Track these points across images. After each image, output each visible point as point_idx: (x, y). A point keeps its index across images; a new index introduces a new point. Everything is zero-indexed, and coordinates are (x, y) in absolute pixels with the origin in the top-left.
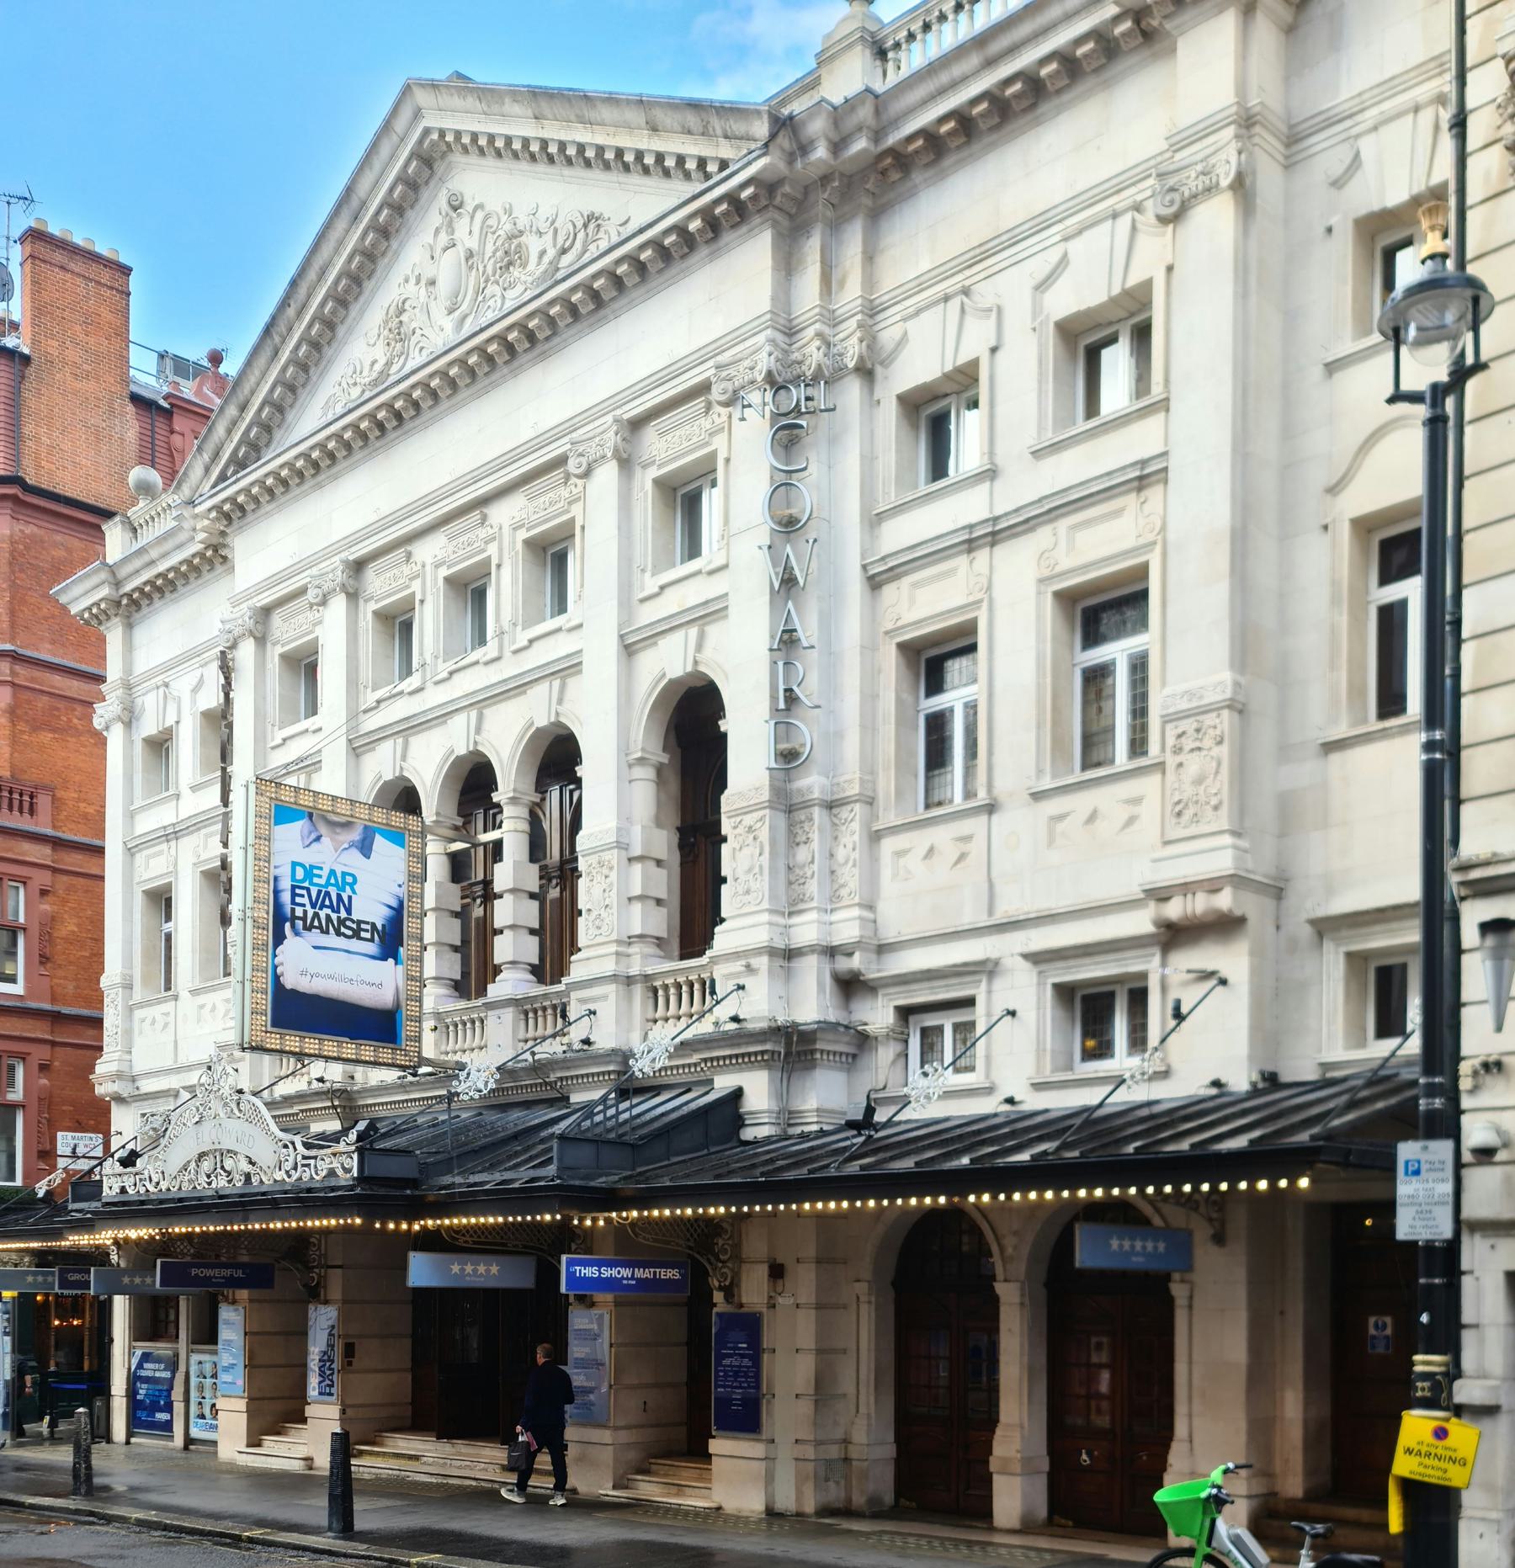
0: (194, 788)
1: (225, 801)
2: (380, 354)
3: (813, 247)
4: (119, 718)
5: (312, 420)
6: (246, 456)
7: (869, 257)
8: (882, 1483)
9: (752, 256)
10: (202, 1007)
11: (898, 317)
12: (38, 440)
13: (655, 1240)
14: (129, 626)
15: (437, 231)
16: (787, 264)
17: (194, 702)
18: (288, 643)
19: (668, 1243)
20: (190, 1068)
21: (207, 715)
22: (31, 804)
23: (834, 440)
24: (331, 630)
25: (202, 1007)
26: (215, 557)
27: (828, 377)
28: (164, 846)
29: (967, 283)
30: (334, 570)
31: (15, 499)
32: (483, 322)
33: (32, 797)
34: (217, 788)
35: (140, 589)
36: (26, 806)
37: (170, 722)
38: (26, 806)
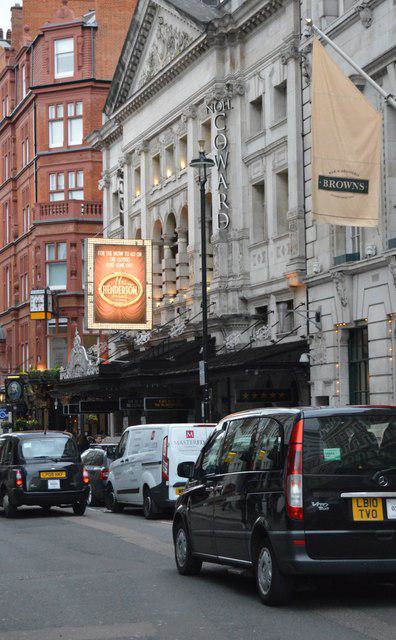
0: (273, 128)
1: (122, 223)
2: (148, 69)
3: (228, 52)
4: (292, 57)
5: (137, 87)
7: (243, 57)
8: (354, 504)
9: (210, 60)
10: (279, 248)
12: (101, 59)
14: (108, 150)
16: (222, 59)
20: (278, 281)
21: (277, 88)
24: (143, 161)
25: (279, 248)
26: (119, 134)
28: (260, 161)
30: (186, 111)
31: (92, 87)
34: (119, 222)
35: (245, 24)
37: (261, 93)
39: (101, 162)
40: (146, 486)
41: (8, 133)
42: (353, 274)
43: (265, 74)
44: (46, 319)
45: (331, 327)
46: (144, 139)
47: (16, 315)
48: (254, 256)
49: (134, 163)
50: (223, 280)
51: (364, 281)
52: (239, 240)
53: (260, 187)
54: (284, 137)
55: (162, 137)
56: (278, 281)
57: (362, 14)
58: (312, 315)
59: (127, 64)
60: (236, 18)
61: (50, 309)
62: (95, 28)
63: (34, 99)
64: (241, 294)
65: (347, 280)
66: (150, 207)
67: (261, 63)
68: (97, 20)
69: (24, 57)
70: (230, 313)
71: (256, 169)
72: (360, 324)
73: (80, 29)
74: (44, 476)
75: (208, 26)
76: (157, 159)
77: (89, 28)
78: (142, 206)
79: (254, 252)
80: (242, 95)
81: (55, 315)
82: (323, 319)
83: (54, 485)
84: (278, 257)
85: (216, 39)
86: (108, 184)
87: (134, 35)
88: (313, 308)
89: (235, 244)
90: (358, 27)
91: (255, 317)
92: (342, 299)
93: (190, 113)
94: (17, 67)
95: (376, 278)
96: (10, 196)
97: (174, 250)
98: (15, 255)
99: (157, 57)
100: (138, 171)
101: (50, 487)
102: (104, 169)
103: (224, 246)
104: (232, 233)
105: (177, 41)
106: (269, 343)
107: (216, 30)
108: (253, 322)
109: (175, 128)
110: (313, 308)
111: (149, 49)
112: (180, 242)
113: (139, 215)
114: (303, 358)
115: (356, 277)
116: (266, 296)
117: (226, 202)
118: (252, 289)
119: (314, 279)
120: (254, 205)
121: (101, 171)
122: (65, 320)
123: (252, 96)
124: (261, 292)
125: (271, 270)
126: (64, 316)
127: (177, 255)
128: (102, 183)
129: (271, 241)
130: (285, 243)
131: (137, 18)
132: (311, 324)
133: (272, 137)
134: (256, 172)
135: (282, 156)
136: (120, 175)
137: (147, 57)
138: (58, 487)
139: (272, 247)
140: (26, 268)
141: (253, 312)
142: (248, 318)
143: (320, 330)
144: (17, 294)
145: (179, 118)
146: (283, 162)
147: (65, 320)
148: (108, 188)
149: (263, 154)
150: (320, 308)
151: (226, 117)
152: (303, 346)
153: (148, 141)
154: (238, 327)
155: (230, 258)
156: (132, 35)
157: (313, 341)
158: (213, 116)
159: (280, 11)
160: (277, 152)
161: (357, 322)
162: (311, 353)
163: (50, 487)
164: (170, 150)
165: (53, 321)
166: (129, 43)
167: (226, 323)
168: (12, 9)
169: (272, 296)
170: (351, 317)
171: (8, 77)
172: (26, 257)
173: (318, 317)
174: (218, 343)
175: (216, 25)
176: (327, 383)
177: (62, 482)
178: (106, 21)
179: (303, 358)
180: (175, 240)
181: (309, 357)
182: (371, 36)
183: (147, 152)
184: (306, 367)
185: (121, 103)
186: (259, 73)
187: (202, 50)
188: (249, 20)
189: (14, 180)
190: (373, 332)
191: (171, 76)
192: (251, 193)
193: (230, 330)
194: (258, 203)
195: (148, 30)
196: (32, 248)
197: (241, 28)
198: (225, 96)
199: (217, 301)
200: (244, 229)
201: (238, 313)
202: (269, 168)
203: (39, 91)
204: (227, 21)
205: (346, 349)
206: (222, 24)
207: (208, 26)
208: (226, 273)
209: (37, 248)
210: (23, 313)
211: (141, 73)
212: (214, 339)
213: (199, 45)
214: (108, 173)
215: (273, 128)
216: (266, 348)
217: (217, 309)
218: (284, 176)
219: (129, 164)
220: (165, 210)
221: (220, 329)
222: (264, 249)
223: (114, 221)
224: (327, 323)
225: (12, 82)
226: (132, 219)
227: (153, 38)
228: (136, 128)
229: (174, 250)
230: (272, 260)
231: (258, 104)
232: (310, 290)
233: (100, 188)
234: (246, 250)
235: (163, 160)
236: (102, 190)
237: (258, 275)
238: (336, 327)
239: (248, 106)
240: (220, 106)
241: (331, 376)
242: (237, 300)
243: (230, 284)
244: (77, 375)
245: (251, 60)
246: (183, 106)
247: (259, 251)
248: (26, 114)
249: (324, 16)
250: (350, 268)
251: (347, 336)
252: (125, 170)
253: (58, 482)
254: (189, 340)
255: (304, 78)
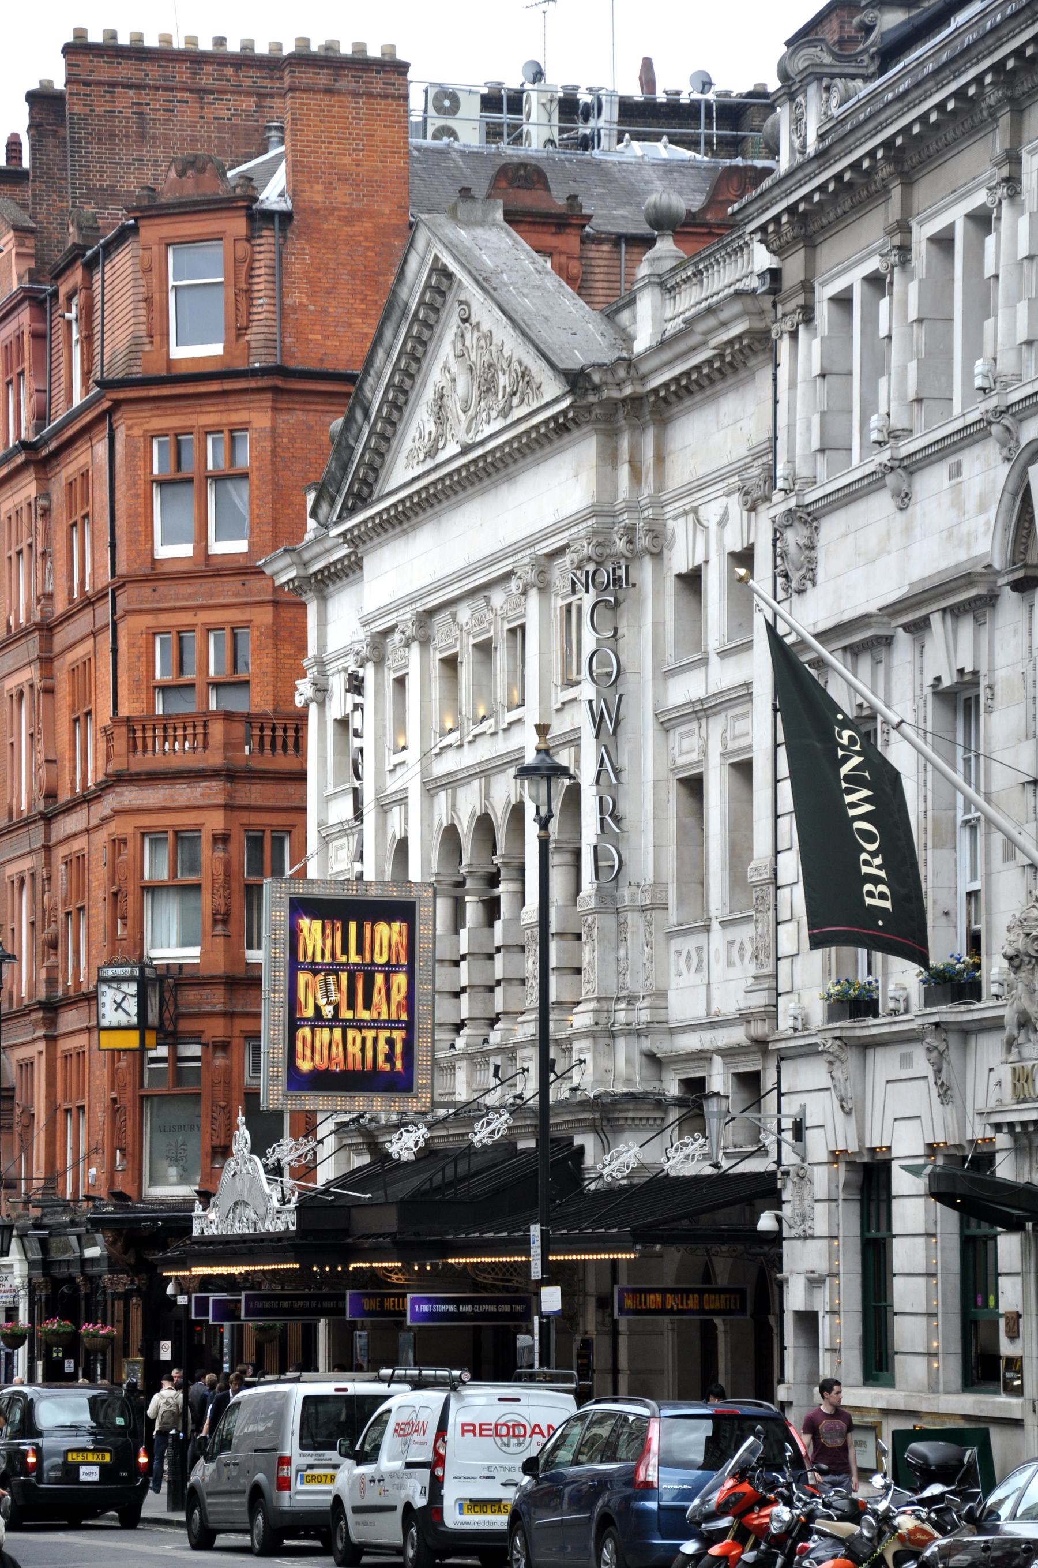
0: (723, 654)
6: (354, 504)
7: (660, 459)
10: (731, 943)
11: (720, 493)
13: (495, 1279)
15: (454, 343)
16: (609, 457)
17: (720, 540)
18: (479, 635)
19: (509, 1281)
20: (726, 1023)
22: (297, 739)
23: (639, 603)
26: (348, 570)
27: (634, 557)
28: (694, 725)
29: (695, 504)
31: (276, 390)
32: (715, 289)
33: (297, 730)
35: (666, 385)
36: (290, 742)
37: (699, 560)
38: (290, 742)
39: (303, 810)
40: (408, 1506)
41: (28, 488)
42: (866, 1046)
43: (711, 513)
44: (143, 1049)
45: (824, 1157)
46: (421, 606)
47: (51, 1022)
48: (679, 953)
49: (392, 661)
50: (605, 1005)
51: (885, 1064)
52: (643, 910)
53: (693, 786)
54: (748, 685)
55: (464, 613)
56: (726, 1023)
57: (890, 479)
58: (787, 1124)
59: (376, 405)
60: (644, 368)
61: (153, 1018)
62: (286, 217)
63: (110, 412)
64: (646, 1044)
65: (851, 1057)
66: (432, 788)
67: (702, 487)
68: (294, 190)
69: (77, 276)
70: (620, 1089)
71: (686, 743)
72: (879, 1157)
73: (238, 225)
74: (72, 1458)
75: (576, 380)
76: (451, 663)
77: (269, 216)
78: (411, 781)
79: (676, 944)
80: (657, 556)
81: (171, 1037)
82: (809, 1134)
83: (89, 1474)
84: (731, 964)
85: (597, 411)
86: (322, 691)
87: (395, 336)
88: (791, 1107)
89: (633, 919)
90: (882, 503)
91: (680, 1102)
92: (842, 1100)
93: (530, 577)
94: (55, 294)
95: (906, 1061)
96: (31, 674)
97: (492, 909)
98: (47, 848)
99: (454, 404)
100: (401, 682)
101: (83, 1477)
102: (312, 650)
103: (609, 921)
104: (626, 892)
105: (503, 380)
106: (709, 1171)
107: (597, 389)
108: (674, 1114)
109: (498, 598)
110: (791, 1107)
111: (435, 377)
112: (505, 889)
113: (403, 801)
114: (766, 1222)
115: (870, 1052)
116: (702, 1056)
117: (611, 816)
118: (672, 1032)
119: (792, 1043)
120: (680, 826)
121: (305, 656)
122: (195, 1050)
123: (679, 562)
124: (690, 1042)
125: (715, 993)
126: (195, 1038)
127: (498, 925)
128: (304, 689)
129: (715, 926)
130: (745, 933)
131: (404, 293)
132: (785, 1147)
133: (723, 676)
134: (684, 749)
135: (741, 726)
136: (356, 685)
137: (429, 395)
138: (96, 1478)
139: (718, 937)
140: (79, 886)
141: (673, 1089)
142: (660, 1104)
143: (803, 1160)
144: (52, 960)
145: (508, 576)
146: (742, 743)
147: (195, 1050)
148: (322, 705)
149: (702, 711)
150: (803, 1108)
151: (617, 603)
152: (765, 1190)
153: (431, 613)
154: (636, 1125)
155: (622, 953)
156: (388, 334)
157: (790, 1186)
158: (588, 600)
159: (743, 374)
160: (732, 713)
161: (872, 1150)
162: (787, 1211)
163: (83, 1477)
164: (485, 649)
165: (163, 1051)
166: (381, 353)
167: (608, 1114)
168: (32, 97)
169: (717, 1060)
170: (861, 1139)
171: (24, 317)
172: (77, 863)
173: (799, 1130)
174: (589, 1160)
175: (596, 378)
176: (815, 1282)
177: (103, 1467)
178: (315, 194)
179: (766, 1222)
180: (493, 880)
181: (779, 1220)
182: (908, 530)
183: (425, 643)
184: (776, 1239)
185: (352, 511)
186: (695, 510)
187: (561, 428)
188: (676, 380)
189: (47, 629)
190: (902, 1182)
191: (486, 471)
192: (673, 797)
193: (619, 1130)
194: (690, 821)
195: (430, 327)
196: (101, 837)
197: (655, 391)
198: (609, 565)
199: (588, 1057)
200: (658, 885)
201: (638, 1088)
202: (715, 749)
203: (121, 395)
204: (622, 373)
205: (855, 1208)
206: (609, 379)
207: (576, 380)
208: (613, 991)
209: (118, 843)
210: (70, 1019)
211: (412, 432)
212: (581, 1149)
213: (554, 418)
214: (321, 664)
215: (723, 654)
216: (697, 1180)
217: (587, 1074)
218: (743, 769)
219: (380, 663)
220: (469, 803)
221: (594, 1128)
222: (700, 939)
223: (334, 796)
224: (818, 1146)
225: (38, 336)
226: (383, 809)
227: (445, 350)
228: (401, 571)
229: (492, 909)
230: (718, 969)
231: (692, 581)
232: (784, 1065)
233: (299, 701)
234: (661, 936)
235: (466, 672)
236: (306, 706)
237: (685, 1003)
238: (835, 1156)
239: (671, 585)
240: (603, 577)
241: (821, 1266)
242: (637, 1058)
243: (621, 1017)
244: (241, 1229)
245: (683, 469)
246: (516, 549)
247: (689, 944)
248: (82, 446)
249: (822, 450)
250: (859, 1033)
251: (857, 1178)
252: (368, 673)
253: (96, 1469)
254: (522, 1145)
255: (780, 580)
